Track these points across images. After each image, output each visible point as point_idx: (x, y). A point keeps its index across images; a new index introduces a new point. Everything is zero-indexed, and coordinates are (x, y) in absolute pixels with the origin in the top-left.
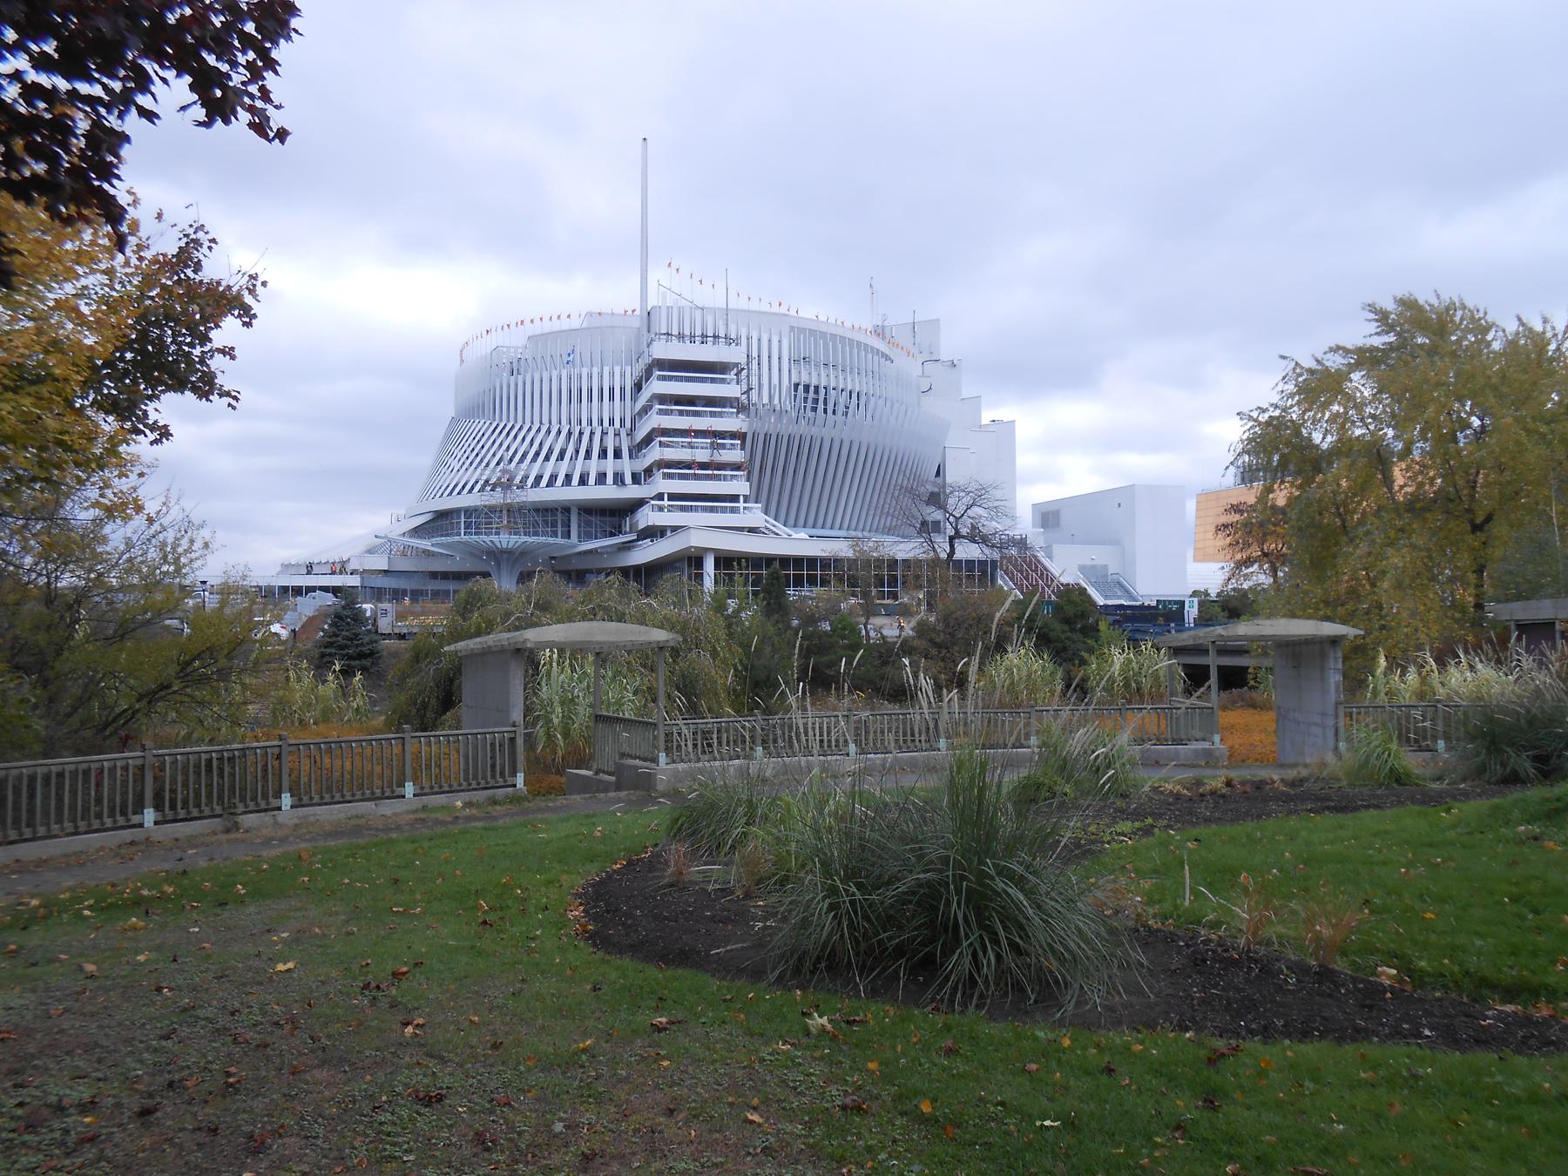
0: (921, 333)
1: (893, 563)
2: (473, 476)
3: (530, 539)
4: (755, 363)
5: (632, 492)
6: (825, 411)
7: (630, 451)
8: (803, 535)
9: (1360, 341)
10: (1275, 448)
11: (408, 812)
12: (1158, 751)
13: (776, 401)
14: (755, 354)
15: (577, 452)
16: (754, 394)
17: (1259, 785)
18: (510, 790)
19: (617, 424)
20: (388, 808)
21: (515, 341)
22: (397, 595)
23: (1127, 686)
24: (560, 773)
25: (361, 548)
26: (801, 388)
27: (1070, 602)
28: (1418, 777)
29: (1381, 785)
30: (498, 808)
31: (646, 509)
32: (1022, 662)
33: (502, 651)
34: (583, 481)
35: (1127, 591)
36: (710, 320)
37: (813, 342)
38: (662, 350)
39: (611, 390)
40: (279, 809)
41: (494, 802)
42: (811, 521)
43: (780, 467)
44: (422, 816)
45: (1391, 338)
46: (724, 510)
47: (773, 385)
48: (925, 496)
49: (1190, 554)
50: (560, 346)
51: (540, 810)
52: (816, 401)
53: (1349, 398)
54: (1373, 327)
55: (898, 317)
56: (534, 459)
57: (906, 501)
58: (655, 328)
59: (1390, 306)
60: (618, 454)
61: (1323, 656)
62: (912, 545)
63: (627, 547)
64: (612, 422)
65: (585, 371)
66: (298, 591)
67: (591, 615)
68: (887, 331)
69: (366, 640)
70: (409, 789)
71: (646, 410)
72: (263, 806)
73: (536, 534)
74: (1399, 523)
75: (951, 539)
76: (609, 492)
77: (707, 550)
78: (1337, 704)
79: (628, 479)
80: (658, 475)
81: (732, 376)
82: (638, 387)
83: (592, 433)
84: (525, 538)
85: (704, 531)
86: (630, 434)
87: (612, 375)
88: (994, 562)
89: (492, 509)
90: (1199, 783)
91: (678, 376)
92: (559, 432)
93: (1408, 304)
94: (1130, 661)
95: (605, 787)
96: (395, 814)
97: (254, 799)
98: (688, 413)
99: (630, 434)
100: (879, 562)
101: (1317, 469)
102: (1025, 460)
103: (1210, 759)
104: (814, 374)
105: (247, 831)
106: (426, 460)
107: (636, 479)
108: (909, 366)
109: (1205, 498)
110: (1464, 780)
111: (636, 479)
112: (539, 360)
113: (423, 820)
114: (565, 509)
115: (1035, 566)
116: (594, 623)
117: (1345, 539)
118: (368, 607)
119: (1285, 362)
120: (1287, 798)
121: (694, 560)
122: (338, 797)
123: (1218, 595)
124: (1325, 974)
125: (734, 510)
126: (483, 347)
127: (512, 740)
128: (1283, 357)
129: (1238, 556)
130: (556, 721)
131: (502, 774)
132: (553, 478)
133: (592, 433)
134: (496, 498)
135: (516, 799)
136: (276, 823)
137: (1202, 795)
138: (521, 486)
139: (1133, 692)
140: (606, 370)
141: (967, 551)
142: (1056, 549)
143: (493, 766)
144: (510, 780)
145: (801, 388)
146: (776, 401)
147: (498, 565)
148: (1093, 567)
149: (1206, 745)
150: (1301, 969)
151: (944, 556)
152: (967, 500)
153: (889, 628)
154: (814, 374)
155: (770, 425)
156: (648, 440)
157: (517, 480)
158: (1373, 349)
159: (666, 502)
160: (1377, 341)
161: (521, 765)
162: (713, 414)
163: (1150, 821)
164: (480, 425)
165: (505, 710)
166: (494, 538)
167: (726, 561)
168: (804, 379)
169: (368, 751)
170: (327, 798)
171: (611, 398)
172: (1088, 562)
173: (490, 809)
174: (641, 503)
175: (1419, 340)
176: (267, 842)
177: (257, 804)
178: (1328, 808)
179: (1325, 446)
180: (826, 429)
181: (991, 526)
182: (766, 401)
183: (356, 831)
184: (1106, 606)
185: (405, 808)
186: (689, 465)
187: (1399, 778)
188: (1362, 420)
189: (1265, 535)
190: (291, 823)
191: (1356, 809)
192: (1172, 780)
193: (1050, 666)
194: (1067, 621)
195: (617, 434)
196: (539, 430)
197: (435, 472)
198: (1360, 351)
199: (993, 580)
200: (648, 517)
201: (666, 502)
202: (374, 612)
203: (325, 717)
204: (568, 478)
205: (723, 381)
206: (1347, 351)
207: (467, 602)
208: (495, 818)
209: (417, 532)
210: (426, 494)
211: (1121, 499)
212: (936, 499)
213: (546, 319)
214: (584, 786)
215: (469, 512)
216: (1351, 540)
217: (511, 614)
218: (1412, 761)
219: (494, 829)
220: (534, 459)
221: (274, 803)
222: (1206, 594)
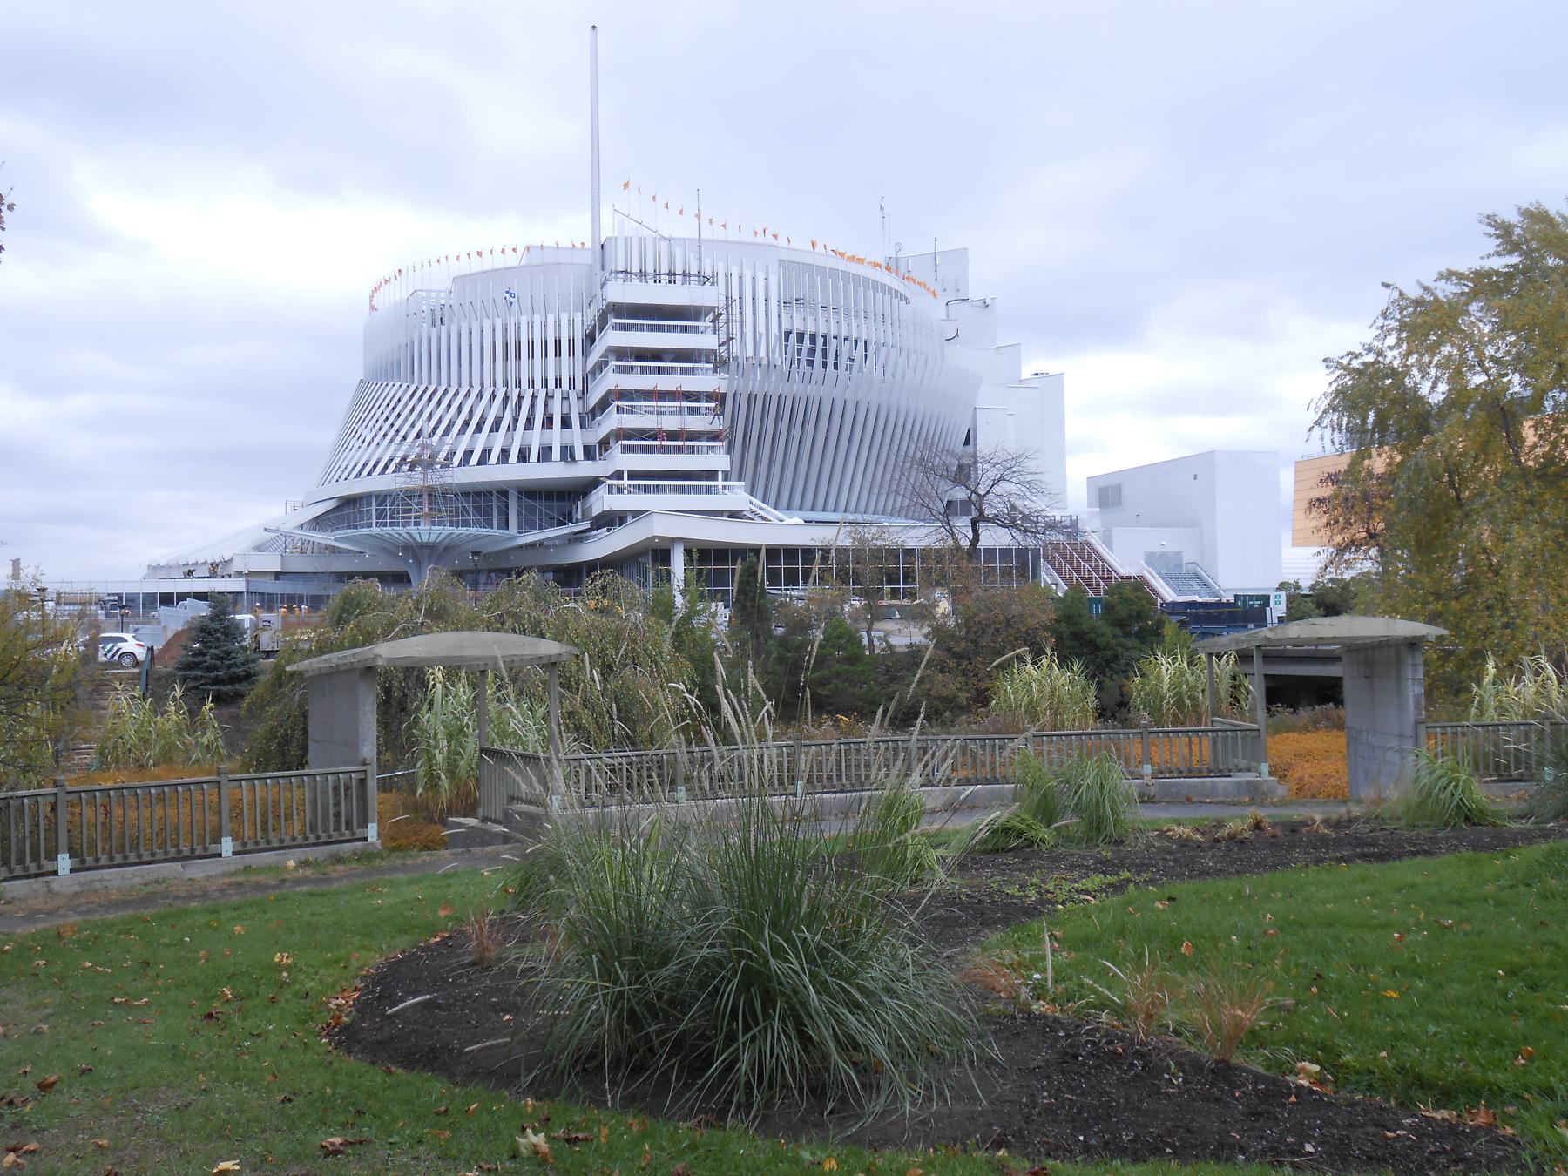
0: (943, 271)
1: (909, 552)
2: (385, 452)
3: (456, 531)
4: (736, 305)
5: (584, 469)
6: (825, 365)
7: (582, 418)
8: (797, 520)
9: (1476, 265)
10: (1369, 400)
11: (225, 874)
12: (1189, 785)
13: (762, 354)
14: (736, 296)
15: (516, 420)
16: (735, 346)
17: (1293, 828)
18: (359, 844)
19: (551, 384)
20: (198, 870)
21: (439, 281)
22: (291, 600)
23: (1179, 703)
24: (444, 823)
25: (245, 545)
26: (793, 337)
27: (1126, 600)
28: (1495, 814)
29: (1447, 824)
30: (340, 867)
31: (601, 491)
32: (1044, 679)
33: (350, 670)
34: (523, 457)
35: (1206, 585)
36: (679, 252)
37: (806, 281)
38: (620, 292)
39: (558, 343)
40: (55, 873)
41: (338, 860)
42: (808, 503)
43: (765, 434)
44: (240, 879)
45: (1515, 259)
46: (698, 490)
47: (757, 336)
48: (950, 472)
49: (1287, 537)
50: (498, 288)
51: (394, 869)
52: (812, 352)
53: (1468, 336)
54: (1492, 244)
55: (915, 247)
56: (462, 431)
57: (915, 476)
58: (610, 266)
59: (1514, 218)
60: (566, 423)
61: (1399, 663)
62: (926, 531)
63: (579, 538)
64: (558, 383)
65: (524, 320)
66: (167, 599)
67: (497, 625)
68: (902, 263)
69: (240, 658)
70: (227, 846)
71: (601, 366)
72: (33, 869)
73: (466, 524)
74: (1526, 493)
75: (974, 523)
76: (555, 471)
77: (674, 540)
78: (1417, 723)
79: (579, 453)
80: (616, 448)
81: (706, 323)
82: (591, 339)
83: (534, 398)
84: (449, 530)
85: (670, 517)
86: (582, 397)
87: (558, 324)
88: (1036, 552)
89: (409, 494)
90: (1220, 824)
91: (644, 325)
92: (493, 396)
93: (1537, 217)
94: (1183, 672)
95: (486, 839)
96: (208, 878)
97: (21, 861)
98: (652, 371)
99: (582, 397)
100: (893, 553)
101: (1425, 429)
102: (1075, 427)
103: (1255, 793)
104: (810, 320)
105: (9, 902)
106: (327, 437)
107: (589, 453)
108: (930, 308)
109: (1302, 466)
110: (1556, 818)
111: (589, 453)
112: (467, 306)
113: (240, 884)
114: (502, 492)
115: (1088, 554)
116: (501, 636)
117: (1459, 513)
118: (245, 619)
119: (1387, 291)
120: (1324, 842)
121: (659, 552)
122: (132, 857)
123: (1312, 588)
124: (1224, 1071)
125: (710, 490)
126: (392, 296)
127: (362, 782)
128: (1386, 286)
129: (1338, 539)
130: (440, 758)
131: (349, 825)
132: (486, 454)
133: (534, 398)
134: (416, 480)
135: (367, 857)
136: (50, 891)
137: (1217, 841)
138: (447, 463)
139: (1185, 712)
140: (551, 318)
141: (993, 537)
142: (1118, 534)
143: (337, 815)
144: (359, 833)
145: (793, 337)
146: (762, 354)
147: (418, 563)
148: (1163, 555)
149: (1251, 776)
150: (1192, 1066)
151: (965, 543)
152: (993, 473)
153: (903, 635)
154: (810, 320)
155: (755, 383)
156: (603, 405)
157: (441, 457)
158: (1490, 273)
159: (626, 482)
160: (1499, 263)
161: (373, 812)
162: (684, 371)
163: (1126, 874)
164: (394, 389)
165: (353, 744)
166: (412, 529)
167: (706, 556)
168: (798, 326)
169: (197, 796)
170: (118, 859)
171: (558, 353)
172: (1157, 549)
173: (329, 869)
174: (595, 483)
175: (1550, 262)
176: (31, 916)
177: (25, 869)
178: (1364, 857)
179: (1437, 398)
180: (825, 387)
181: (1034, 504)
182: (750, 353)
183: (149, 900)
184: (1174, 604)
185: (221, 869)
186: (653, 435)
187: (1470, 817)
188: (1481, 364)
189: (1371, 510)
190: (69, 890)
191: (1400, 857)
192: (1179, 823)
193: (1081, 681)
194: (1121, 624)
195: (565, 398)
196: (468, 394)
197: (343, 445)
198: (1478, 275)
199: (1036, 575)
200: (603, 501)
201: (626, 482)
202: (255, 626)
203: (166, 757)
204: (505, 453)
205: (696, 330)
206: (1460, 276)
207: (343, 610)
208: (329, 881)
209: (318, 522)
210: (328, 476)
211: (1198, 468)
212: (963, 474)
213: (497, 252)
214: (470, 839)
215: (382, 497)
216: (1467, 515)
217: (397, 623)
218: (1483, 793)
219: (322, 895)
220: (462, 431)
221: (48, 866)
222: (1297, 587)
